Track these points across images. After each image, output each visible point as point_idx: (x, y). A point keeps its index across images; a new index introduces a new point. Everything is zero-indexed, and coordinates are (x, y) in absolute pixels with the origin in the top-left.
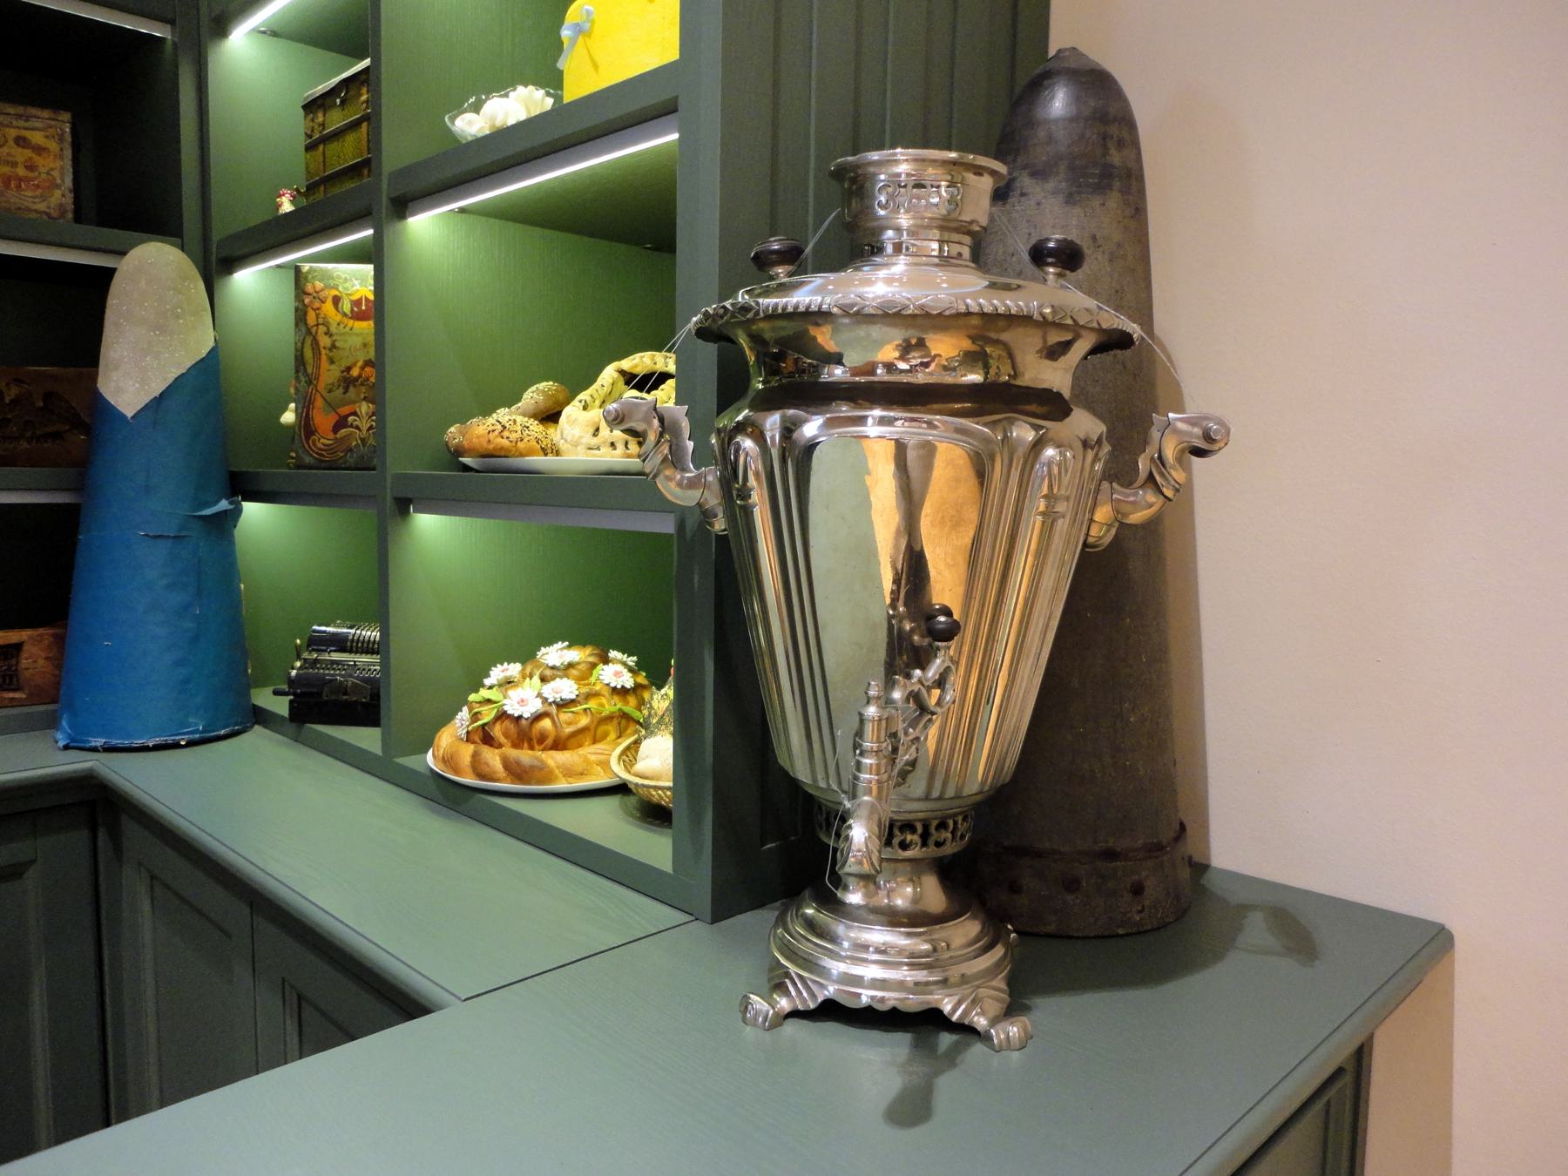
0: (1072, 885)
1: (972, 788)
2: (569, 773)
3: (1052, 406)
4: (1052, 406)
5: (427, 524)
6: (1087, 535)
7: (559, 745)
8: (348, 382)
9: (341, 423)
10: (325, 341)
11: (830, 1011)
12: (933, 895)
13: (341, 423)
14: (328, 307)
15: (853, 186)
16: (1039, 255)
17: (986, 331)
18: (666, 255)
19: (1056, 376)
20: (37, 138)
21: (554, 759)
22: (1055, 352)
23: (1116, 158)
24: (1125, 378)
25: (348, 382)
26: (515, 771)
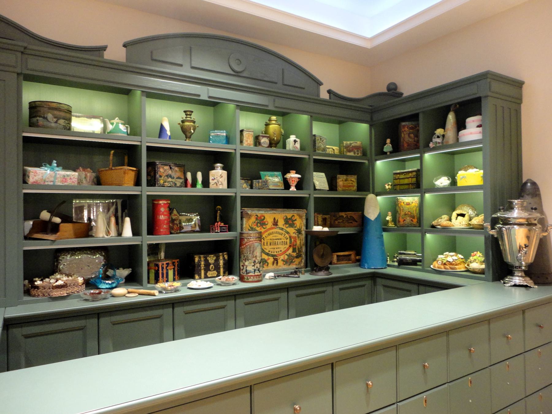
0: (538, 277)
1: (530, 262)
2: (459, 269)
3: (536, 225)
4: (536, 225)
5: (428, 236)
6: (193, 232)
7: (456, 265)
8: (405, 214)
9: (404, 220)
10: (402, 208)
11: (515, 285)
12: (524, 275)
13: (404, 220)
14: (402, 204)
15: (511, 203)
16: (532, 209)
17: (527, 219)
18: (456, 197)
19: (536, 222)
20: (353, 179)
21: (456, 267)
22: (535, 220)
23: (537, 193)
24: (542, 222)
25: (405, 214)
26: (451, 268)
